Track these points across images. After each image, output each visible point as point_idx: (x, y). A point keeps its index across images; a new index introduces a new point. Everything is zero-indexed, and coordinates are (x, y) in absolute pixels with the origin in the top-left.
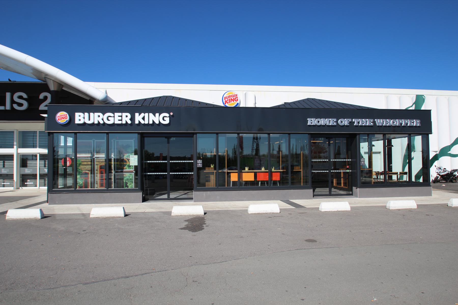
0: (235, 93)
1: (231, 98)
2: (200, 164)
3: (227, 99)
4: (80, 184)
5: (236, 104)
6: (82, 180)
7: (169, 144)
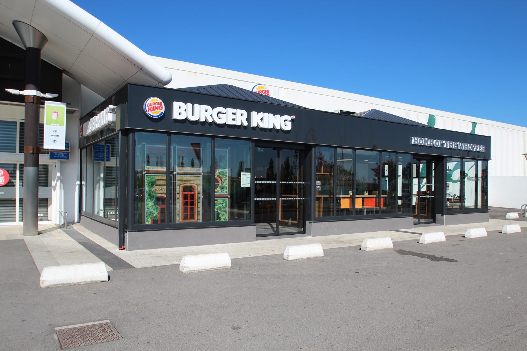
0: (266, 88)
1: (156, 105)
2: (318, 187)
3: (151, 106)
4: (153, 216)
5: (160, 113)
6: (157, 209)
7: (279, 158)
